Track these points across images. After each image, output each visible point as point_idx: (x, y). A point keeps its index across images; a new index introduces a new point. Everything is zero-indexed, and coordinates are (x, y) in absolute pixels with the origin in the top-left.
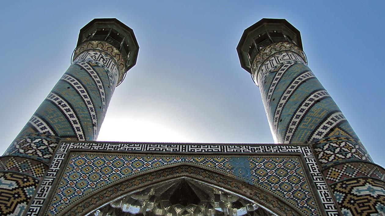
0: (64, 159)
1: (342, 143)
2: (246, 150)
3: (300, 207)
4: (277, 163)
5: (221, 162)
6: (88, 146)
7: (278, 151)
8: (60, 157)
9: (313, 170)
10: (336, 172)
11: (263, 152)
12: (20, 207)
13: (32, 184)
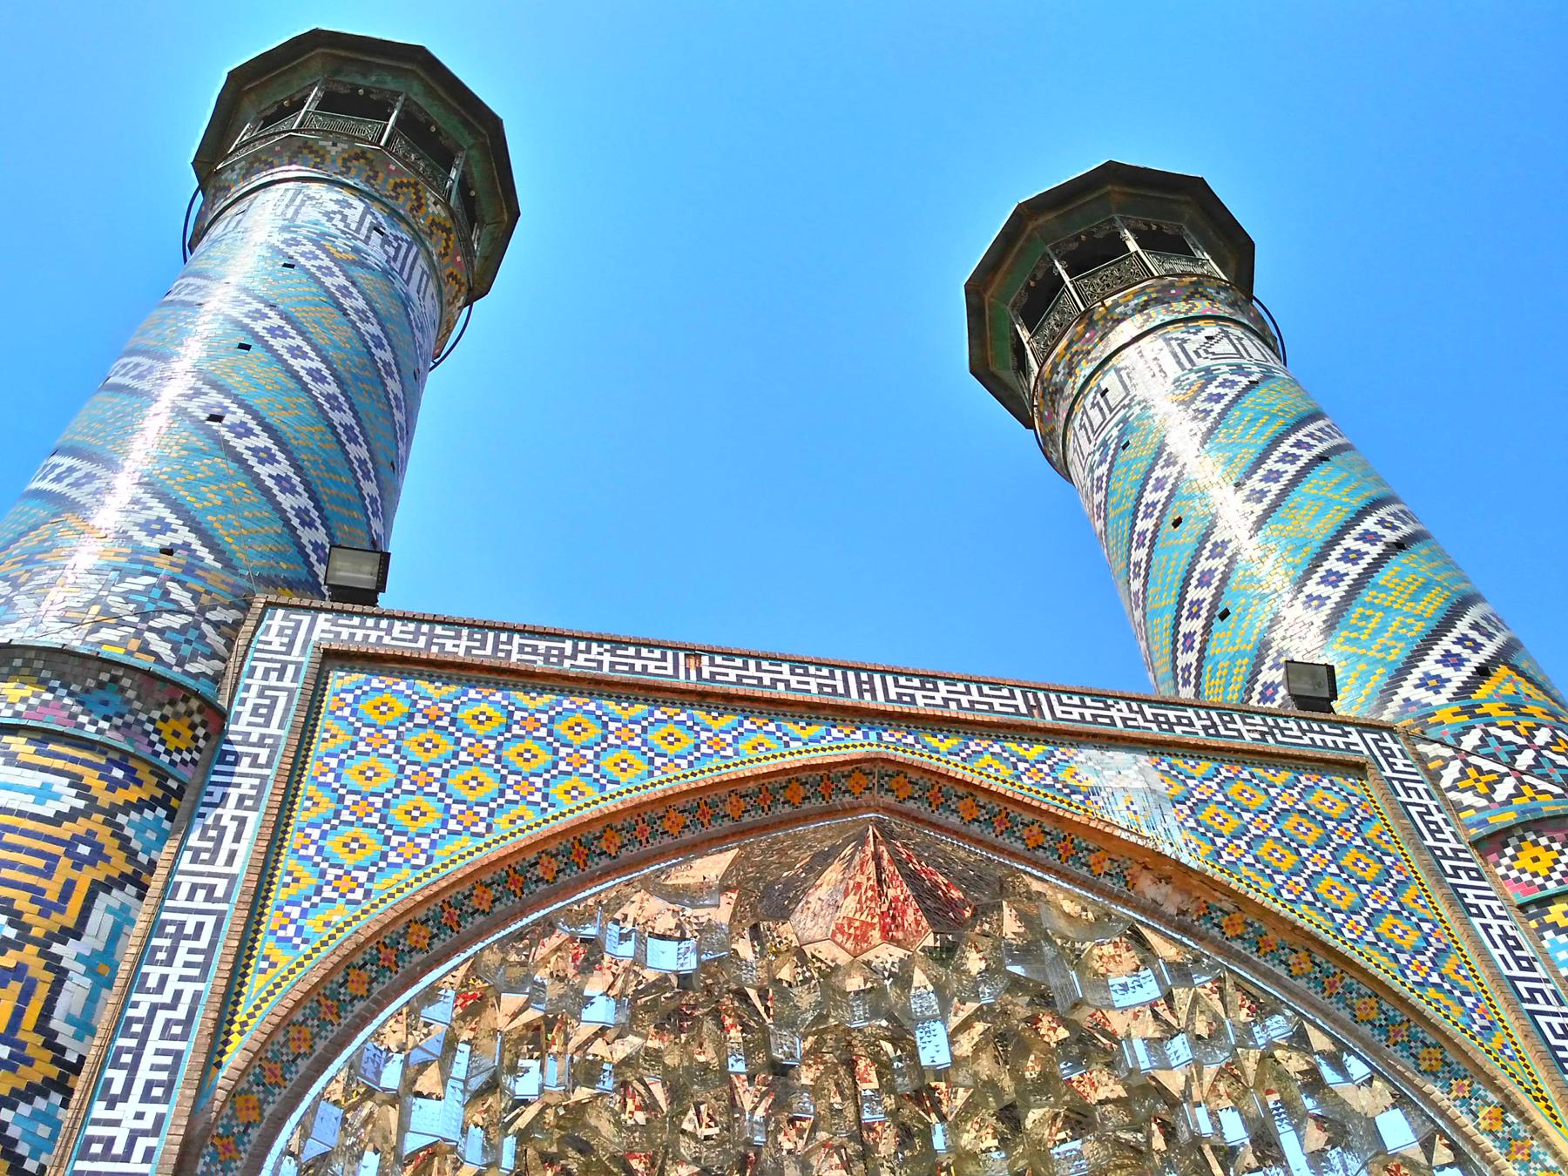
2: (1135, 720)
3: (1414, 982)
6: (411, 637)
8: (274, 675)
9: (1432, 832)
12: (109, 909)
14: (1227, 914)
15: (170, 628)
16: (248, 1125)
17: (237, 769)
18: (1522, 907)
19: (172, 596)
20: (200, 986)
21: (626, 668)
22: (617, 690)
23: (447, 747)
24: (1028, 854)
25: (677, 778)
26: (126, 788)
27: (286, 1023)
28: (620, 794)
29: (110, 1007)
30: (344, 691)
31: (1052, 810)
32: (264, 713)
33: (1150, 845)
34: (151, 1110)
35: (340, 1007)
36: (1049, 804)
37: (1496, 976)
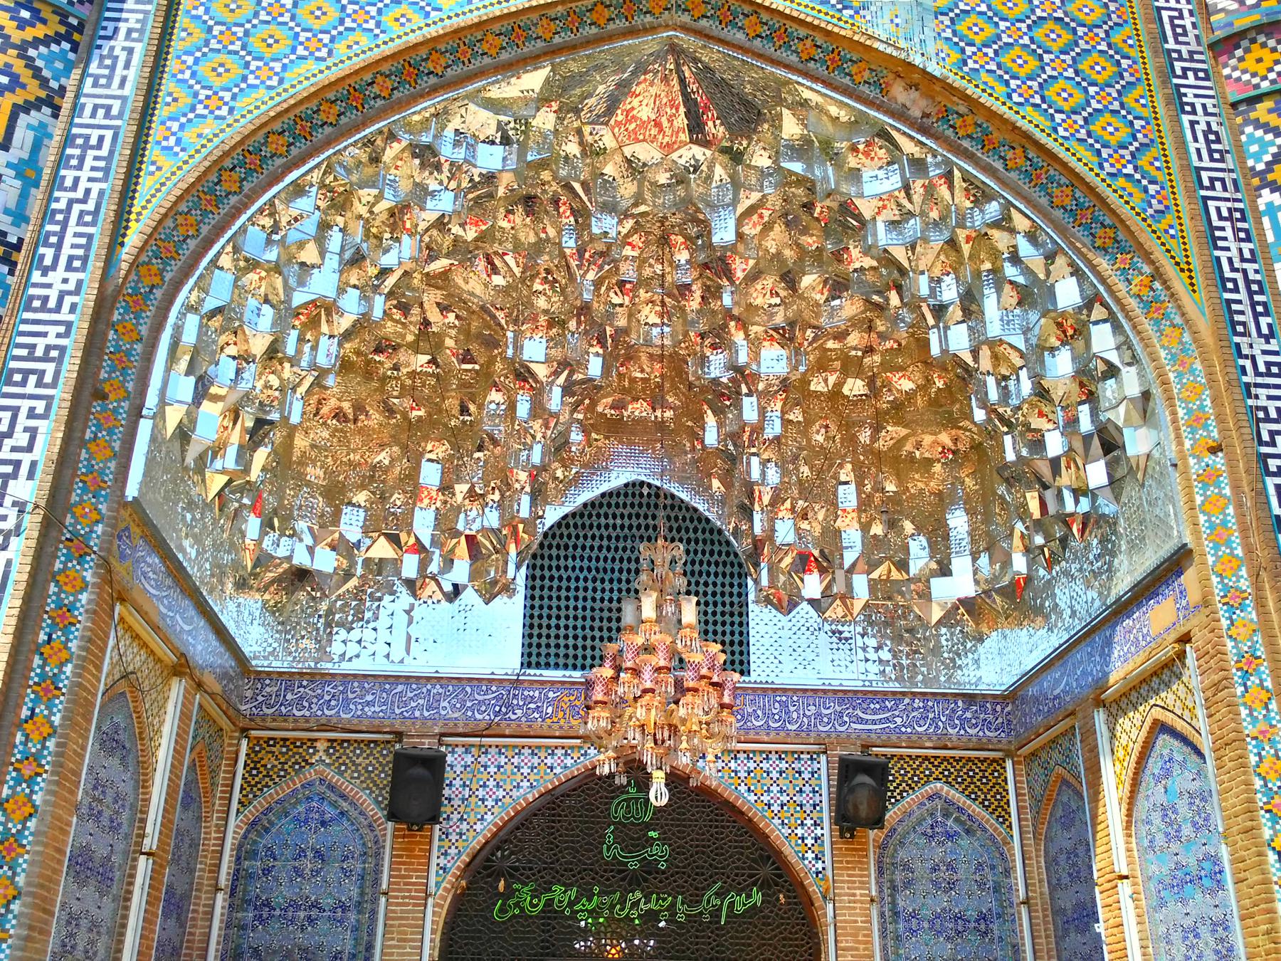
9: (1176, 35)
10: (1267, 50)
12: (29, 126)
14: (962, 116)
16: (153, 287)
17: (126, 6)
18: (1234, 105)
20: (104, 185)
24: (801, 66)
26: (33, 26)
28: (442, 20)
29: (39, 202)
31: (823, 25)
33: (903, 56)
35: (218, 202)
37: (1186, 166)
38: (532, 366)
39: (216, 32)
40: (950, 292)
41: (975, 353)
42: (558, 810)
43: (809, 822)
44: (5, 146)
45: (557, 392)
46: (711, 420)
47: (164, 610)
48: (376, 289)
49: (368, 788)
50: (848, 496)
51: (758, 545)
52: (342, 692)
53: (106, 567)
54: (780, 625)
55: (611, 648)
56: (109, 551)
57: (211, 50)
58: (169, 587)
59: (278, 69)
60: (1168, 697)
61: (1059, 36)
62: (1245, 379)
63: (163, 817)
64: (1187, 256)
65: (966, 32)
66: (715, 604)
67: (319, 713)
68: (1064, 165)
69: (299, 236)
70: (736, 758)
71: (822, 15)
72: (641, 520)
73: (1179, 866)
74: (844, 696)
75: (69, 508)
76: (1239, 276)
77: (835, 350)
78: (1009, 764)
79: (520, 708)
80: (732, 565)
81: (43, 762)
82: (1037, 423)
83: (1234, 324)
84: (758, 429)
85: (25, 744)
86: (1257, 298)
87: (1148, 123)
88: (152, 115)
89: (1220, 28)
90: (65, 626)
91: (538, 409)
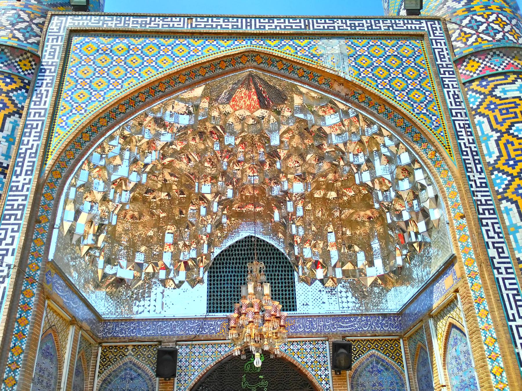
0: (61, 43)
1: (491, 15)
2: (343, 26)
4: (388, 47)
5: (304, 46)
6: (97, 22)
7: (391, 28)
8: (55, 40)
9: (441, 58)
10: (475, 62)
11: (368, 29)
12: (11, 122)
13: (20, 86)
15: (21, 28)
16: (58, 179)
17: (46, 74)
18: (464, 84)
19: (21, 16)
20: (38, 142)
21: (167, 26)
22: (164, 34)
23: (109, 60)
24: (299, 79)
25: (182, 64)
26: (11, 84)
27: (64, 150)
28: (163, 72)
30: (77, 44)
32: (52, 54)
33: (336, 73)
34: (28, 178)
35: (81, 145)
36: (306, 62)
38: (205, 195)
39: (79, 82)
40: (361, 159)
41: (373, 181)
42: (224, 369)
43: (323, 369)
44: (2, 130)
45: (215, 204)
46: (276, 212)
47: (65, 300)
48: (143, 172)
49: (149, 364)
50: (332, 238)
51: (297, 258)
52: (137, 326)
53: (41, 286)
54: (308, 290)
55: (237, 305)
56: (43, 281)
57: (78, 89)
58: (67, 291)
59: (103, 94)
60: (453, 313)
61: (396, 62)
62: (472, 189)
63: (68, 381)
64: (448, 143)
65: (360, 63)
66: (282, 283)
67: (129, 335)
68: (399, 111)
69: (113, 154)
70: (293, 344)
71: (305, 60)
72: (252, 251)
73: (463, 381)
74: (335, 317)
75: (27, 266)
76: (468, 150)
77: (323, 181)
78: (401, 341)
79: (207, 329)
80: (288, 267)
81: (19, 364)
82: (398, 207)
83: (467, 168)
84: (295, 213)
85: (12, 357)
86: (476, 157)
87: (431, 93)
88: (56, 115)
89: (458, 54)
90: (26, 311)
91: (209, 212)
